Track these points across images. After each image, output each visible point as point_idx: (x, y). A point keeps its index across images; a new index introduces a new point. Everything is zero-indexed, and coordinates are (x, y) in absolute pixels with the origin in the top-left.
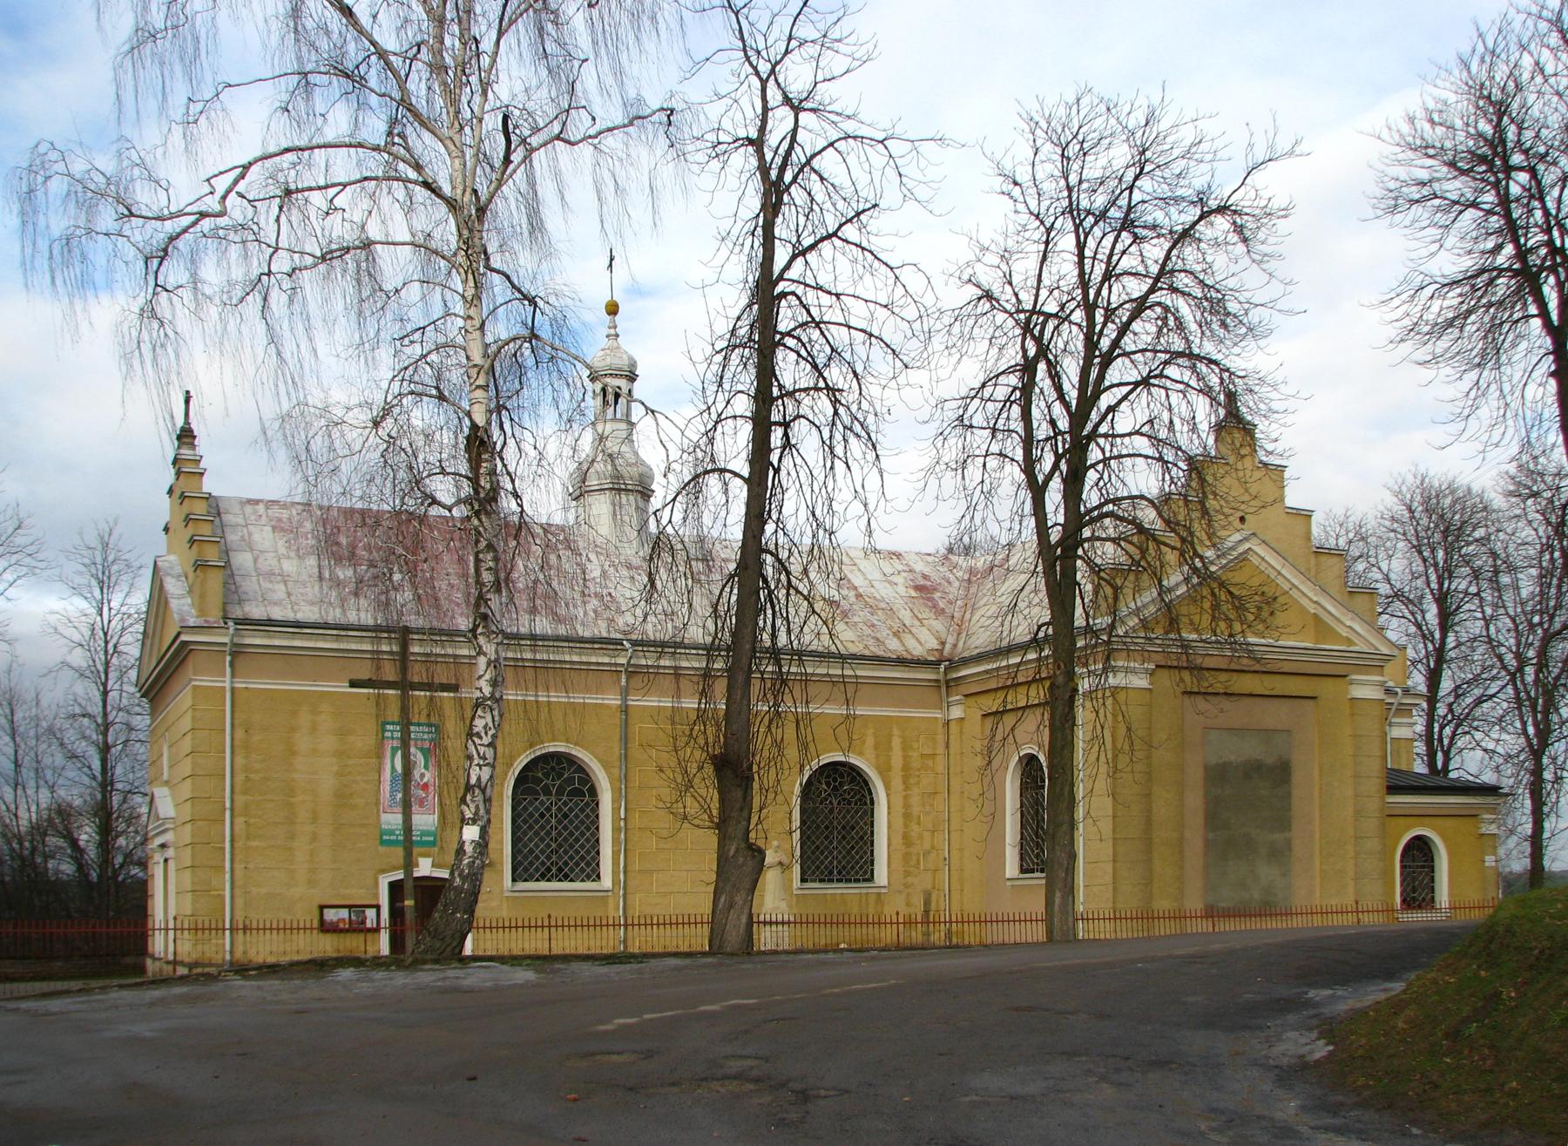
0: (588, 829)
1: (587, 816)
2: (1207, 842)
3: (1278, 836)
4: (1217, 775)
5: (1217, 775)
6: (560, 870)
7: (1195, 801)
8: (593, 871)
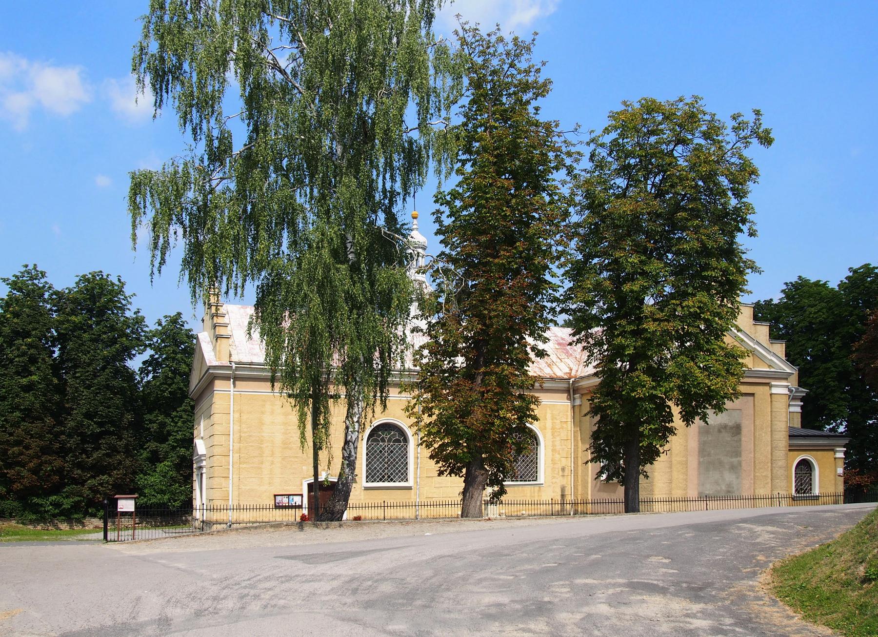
2: (699, 463)
3: (735, 460)
6: (389, 477)
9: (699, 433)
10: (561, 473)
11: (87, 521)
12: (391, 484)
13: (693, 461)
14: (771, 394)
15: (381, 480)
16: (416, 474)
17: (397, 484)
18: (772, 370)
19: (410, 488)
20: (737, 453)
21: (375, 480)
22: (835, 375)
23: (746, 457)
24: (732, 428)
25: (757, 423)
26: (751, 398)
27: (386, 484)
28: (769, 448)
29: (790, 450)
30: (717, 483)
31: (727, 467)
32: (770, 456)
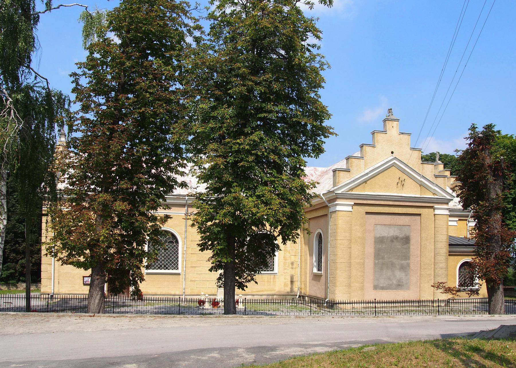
0: (175, 253)
1: (175, 250)
2: (375, 264)
3: (404, 262)
4: (380, 241)
5: (380, 241)
6: (165, 266)
7: (370, 250)
8: (176, 266)
9: (375, 242)
10: (290, 266)
11: (19, 285)
12: (167, 271)
13: (370, 263)
14: (435, 215)
15: (159, 268)
16: (183, 264)
17: (171, 271)
18: (436, 197)
19: (179, 274)
20: (407, 257)
21: (155, 268)
22: (510, 200)
23: (414, 261)
24: (402, 239)
25: (423, 235)
26: (419, 217)
27: (163, 271)
28: (433, 254)
29: (449, 255)
30: (389, 279)
31: (398, 267)
32: (433, 260)
